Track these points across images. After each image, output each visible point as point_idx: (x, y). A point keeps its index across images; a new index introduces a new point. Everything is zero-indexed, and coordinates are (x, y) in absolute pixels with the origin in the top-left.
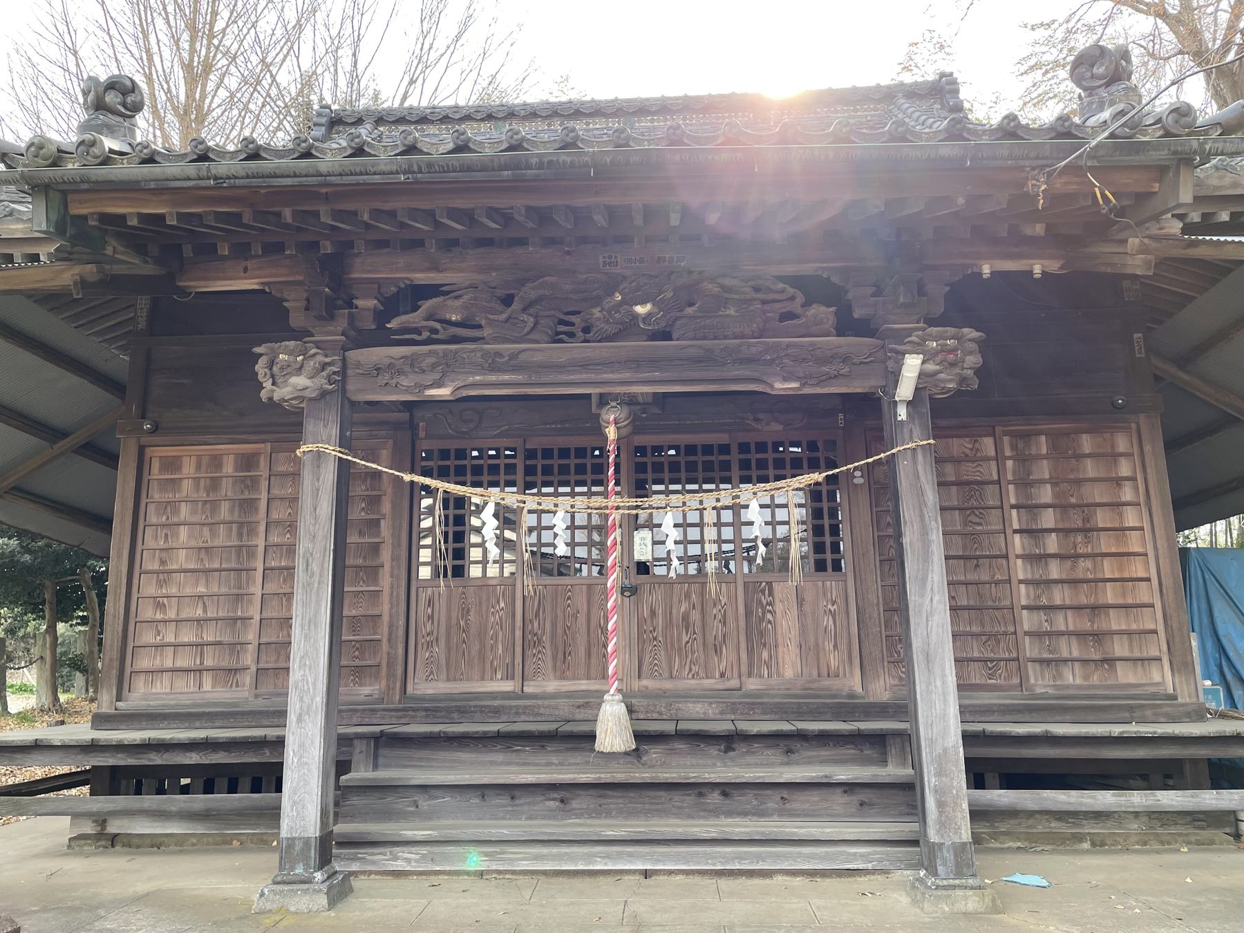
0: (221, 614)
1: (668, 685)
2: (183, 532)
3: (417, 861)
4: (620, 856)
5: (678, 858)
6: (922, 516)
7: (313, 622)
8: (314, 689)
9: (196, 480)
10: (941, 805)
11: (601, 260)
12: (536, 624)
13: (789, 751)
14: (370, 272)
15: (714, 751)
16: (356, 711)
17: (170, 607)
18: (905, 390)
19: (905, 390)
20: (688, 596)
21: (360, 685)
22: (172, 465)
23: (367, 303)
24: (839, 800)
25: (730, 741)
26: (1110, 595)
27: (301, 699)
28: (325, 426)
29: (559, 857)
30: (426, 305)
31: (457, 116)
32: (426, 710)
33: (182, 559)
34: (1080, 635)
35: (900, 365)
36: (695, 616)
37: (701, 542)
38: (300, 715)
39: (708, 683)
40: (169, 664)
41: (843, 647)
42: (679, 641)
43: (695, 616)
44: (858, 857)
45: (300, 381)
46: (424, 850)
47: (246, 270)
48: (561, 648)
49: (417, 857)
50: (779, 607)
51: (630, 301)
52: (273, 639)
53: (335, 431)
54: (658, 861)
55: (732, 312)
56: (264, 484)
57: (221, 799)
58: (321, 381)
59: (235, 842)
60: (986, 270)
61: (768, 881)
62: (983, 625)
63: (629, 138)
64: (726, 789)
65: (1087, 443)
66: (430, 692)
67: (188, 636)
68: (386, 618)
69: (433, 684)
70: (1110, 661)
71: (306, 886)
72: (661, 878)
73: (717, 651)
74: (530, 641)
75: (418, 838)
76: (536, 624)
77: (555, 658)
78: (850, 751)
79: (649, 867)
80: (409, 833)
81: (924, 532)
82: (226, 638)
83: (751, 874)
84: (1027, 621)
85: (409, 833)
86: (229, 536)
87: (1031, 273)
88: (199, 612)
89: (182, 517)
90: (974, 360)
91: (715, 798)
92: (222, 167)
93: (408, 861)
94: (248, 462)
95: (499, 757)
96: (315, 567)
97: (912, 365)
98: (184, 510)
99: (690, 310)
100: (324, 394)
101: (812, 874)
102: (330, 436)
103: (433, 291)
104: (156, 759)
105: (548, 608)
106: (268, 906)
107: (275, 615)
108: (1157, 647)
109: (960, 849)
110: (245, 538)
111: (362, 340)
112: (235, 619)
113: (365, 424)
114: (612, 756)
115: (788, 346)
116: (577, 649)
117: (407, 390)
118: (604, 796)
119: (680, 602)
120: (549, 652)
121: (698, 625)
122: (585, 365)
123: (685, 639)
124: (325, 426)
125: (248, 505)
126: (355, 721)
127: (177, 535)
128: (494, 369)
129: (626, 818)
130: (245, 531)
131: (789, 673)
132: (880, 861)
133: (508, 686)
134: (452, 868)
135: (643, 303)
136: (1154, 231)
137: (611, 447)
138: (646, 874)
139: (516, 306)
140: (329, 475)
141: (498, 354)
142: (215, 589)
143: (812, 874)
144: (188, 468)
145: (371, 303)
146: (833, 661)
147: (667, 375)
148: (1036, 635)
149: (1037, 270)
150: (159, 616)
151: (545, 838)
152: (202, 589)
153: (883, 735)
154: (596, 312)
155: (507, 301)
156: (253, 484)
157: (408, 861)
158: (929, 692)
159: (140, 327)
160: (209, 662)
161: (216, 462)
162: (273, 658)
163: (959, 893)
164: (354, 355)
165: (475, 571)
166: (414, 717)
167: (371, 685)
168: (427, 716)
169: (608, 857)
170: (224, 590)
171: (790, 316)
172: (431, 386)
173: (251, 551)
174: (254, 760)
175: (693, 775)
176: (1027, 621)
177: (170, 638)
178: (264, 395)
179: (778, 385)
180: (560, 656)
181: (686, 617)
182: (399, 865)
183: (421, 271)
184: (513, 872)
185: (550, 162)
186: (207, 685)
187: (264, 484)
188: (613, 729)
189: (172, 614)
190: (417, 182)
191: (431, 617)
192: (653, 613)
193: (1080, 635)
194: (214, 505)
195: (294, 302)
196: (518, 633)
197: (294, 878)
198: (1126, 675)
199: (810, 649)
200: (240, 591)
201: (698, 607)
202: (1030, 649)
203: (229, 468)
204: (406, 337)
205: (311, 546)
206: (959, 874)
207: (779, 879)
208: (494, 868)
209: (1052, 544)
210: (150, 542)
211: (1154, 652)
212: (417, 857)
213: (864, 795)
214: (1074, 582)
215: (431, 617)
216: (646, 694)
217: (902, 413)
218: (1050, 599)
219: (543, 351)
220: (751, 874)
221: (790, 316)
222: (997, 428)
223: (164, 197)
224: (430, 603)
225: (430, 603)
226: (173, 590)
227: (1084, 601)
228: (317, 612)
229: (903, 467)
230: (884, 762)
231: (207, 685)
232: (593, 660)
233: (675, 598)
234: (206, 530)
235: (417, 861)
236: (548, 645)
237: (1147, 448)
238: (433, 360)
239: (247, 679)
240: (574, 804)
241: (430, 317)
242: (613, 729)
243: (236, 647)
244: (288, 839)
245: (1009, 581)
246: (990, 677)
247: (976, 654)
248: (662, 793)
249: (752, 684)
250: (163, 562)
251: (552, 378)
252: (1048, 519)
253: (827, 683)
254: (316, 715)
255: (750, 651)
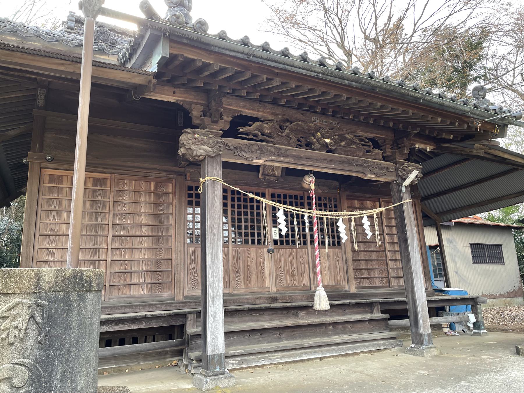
0: (87, 258)
3: (236, 364)
5: (332, 351)
6: (411, 225)
8: (218, 286)
11: (313, 119)
12: (236, 264)
14: (229, 105)
16: (162, 304)
17: (57, 253)
19: (407, 183)
20: (291, 254)
21: (162, 292)
27: (213, 291)
28: (216, 170)
29: (290, 356)
32: (195, 302)
36: (294, 262)
38: (213, 298)
41: (342, 273)
42: (289, 272)
46: (239, 359)
47: (174, 92)
48: (246, 274)
49: (236, 362)
51: (323, 137)
52: (117, 271)
54: (323, 353)
57: (128, 348)
59: (105, 373)
60: (417, 146)
61: (358, 356)
62: (378, 266)
63: (389, 80)
66: (194, 294)
69: (195, 291)
71: (223, 376)
72: (326, 359)
73: (302, 275)
75: (236, 354)
76: (236, 264)
77: (244, 278)
79: (321, 356)
80: (232, 352)
81: (412, 231)
83: (353, 354)
85: (232, 352)
86: (91, 219)
87: (426, 150)
89: (64, 207)
92: (270, 55)
93: (233, 364)
95: (247, 319)
96: (215, 231)
101: (370, 352)
102: (218, 174)
103: (256, 120)
105: (241, 258)
106: (211, 387)
107: (118, 259)
109: (429, 335)
110: (100, 220)
112: (95, 261)
113: (165, 171)
115: (371, 162)
117: (246, 159)
118: (294, 331)
119: (289, 256)
121: (295, 265)
122: (311, 159)
123: (291, 271)
124: (216, 170)
126: (163, 308)
127: (61, 216)
128: (278, 155)
129: (302, 339)
130: (99, 217)
132: (388, 345)
134: (251, 365)
135: (328, 138)
136: (486, 143)
137: (248, 194)
138: (321, 359)
143: (370, 352)
147: (336, 167)
149: (428, 149)
150: (50, 258)
151: (285, 349)
157: (233, 364)
158: (418, 284)
159: (40, 105)
162: (118, 280)
163: (432, 349)
166: (190, 306)
167: (167, 292)
168: (196, 305)
169: (307, 353)
170: (88, 246)
172: (256, 158)
174: (137, 327)
179: (369, 176)
180: (246, 278)
181: (291, 262)
183: (249, 109)
184: (275, 364)
185: (369, 82)
188: (321, 301)
190: (317, 78)
191: (193, 261)
195: (196, 113)
197: (217, 373)
200: (97, 247)
201: (295, 258)
204: (244, 136)
205: (213, 222)
206: (429, 344)
207: (362, 355)
208: (267, 363)
212: (236, 362)
213: (373, 323)
215: (193, 261)
218: (396, 257)
220: (353, 354)
222: (381, 199)
223: (212, 56)
228: (217, 252)
229: (405, 207)
230: (372, 312)
232: (259, 279)
233: (287, 255)
235: (236, 364)
236: (241, 274)
238: (257, 147)
241: (258, 129)
242: (321, 301)
244: (211, 355)
245: (385, 251)
246: (381, 283)
247: (377, 276)
248: (313, 328)
250: (52, 230)
251: (303, 162)
254: (220, 298)
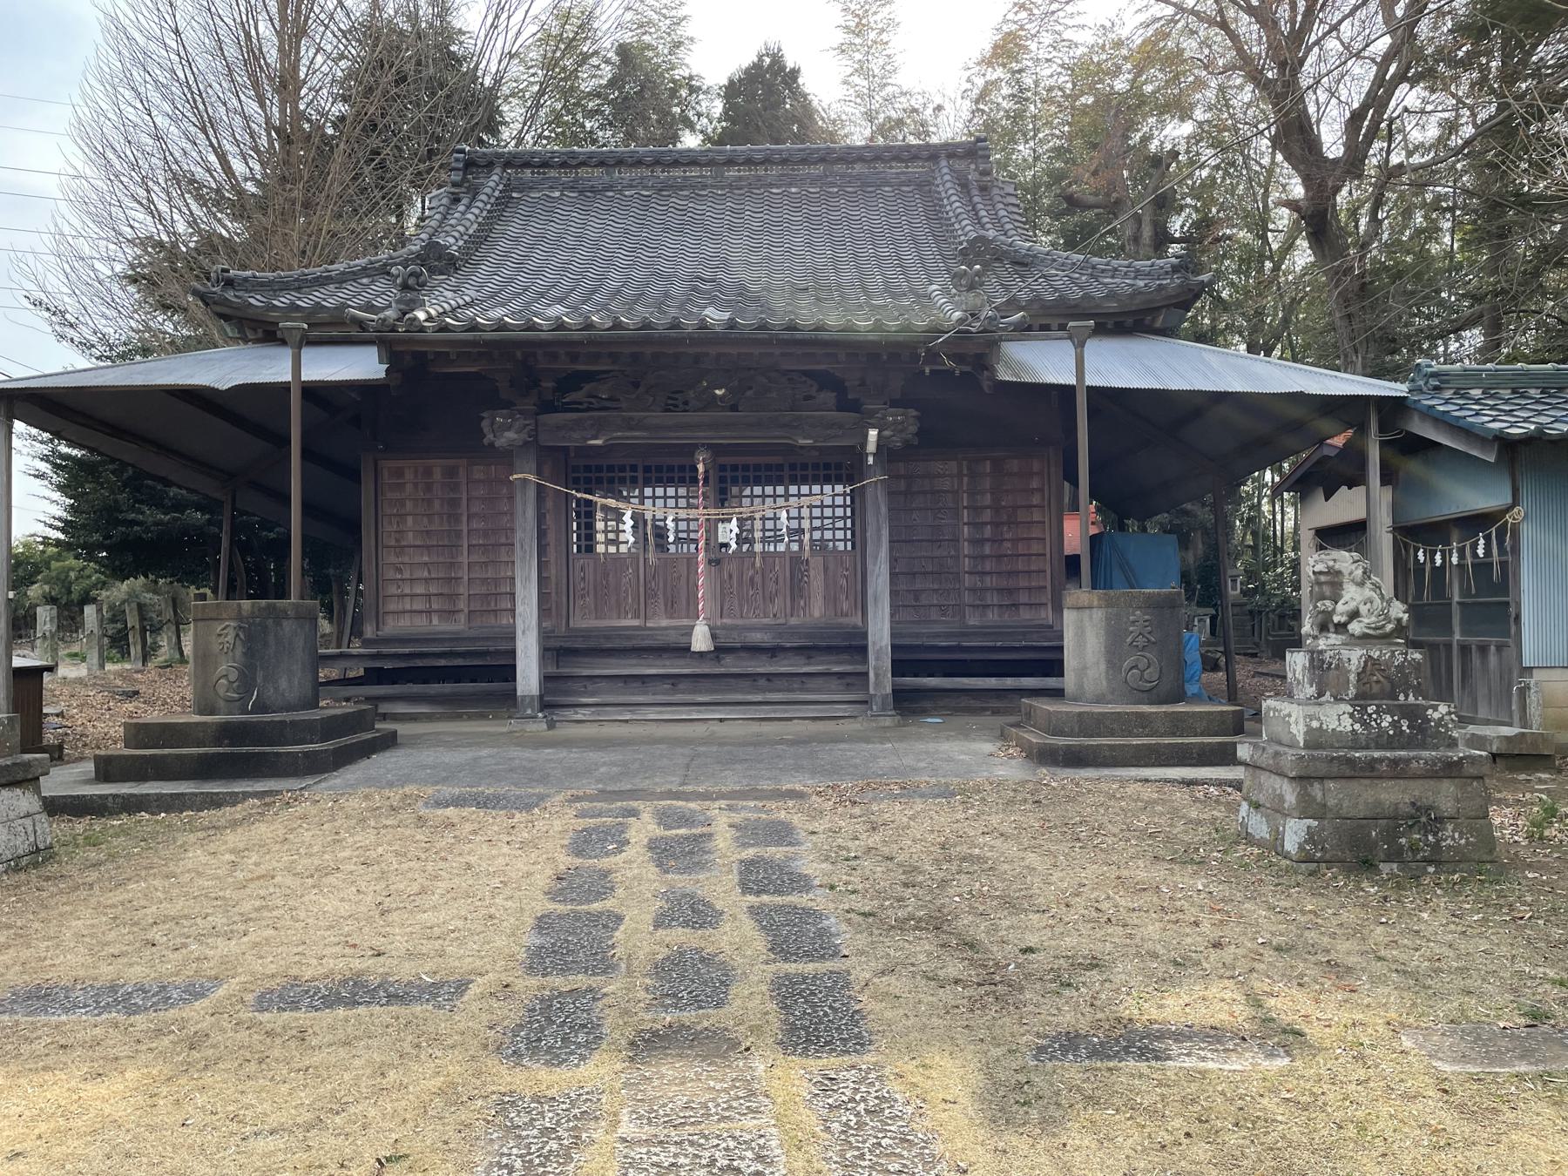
1: (740, 622)
2: (410, 520)
4: (706, 712)
7: (528, 579)
9: (416, 485)
10: (877, 675)
13: (809, 658)
15: (764, 657)
18: (871, 447)
19: (871, 447)
22: (399, 473)
23: (548, 384)
24: (834, 683)
25: (773, 651)
26: (1020, 565)
30: (587, 387)
31: (574, 162)
33: (410, 538)
34: (1000, 590)
35: (867, 436)
36: (758, 579)
37: (812, 518)
39: (766, 621)
40: (408, 607)
41: (852, 598)
43: (758, 579)
44: (840, 710)
45: (511, 435)
50: (812, 573)
53: (534, 466)
55: (774, 395)
56: (464, 488)
58: (524, 436)
64: (769, 677)
65: (1014, 465)
67: (420, 590)
68: (553, 579)
70: (1016, 606)
73: (772, 601)
74: (650, 594)
78: (846, 657)
81: (879, 530)
82: (446, 591)
84: (968, 581)
88: (426, 574)
90: (913, 429)
91: (762, 682)
94: (451, 472)
95: (634, 662)
97: (873, 433)
98: (409, 505)
99: (749, 393)
100: (526, 443)
104: (419, 663)
108: (1047, 597)
111: (548, 407)
114: (701, 654)
116: (682, 602)
120: (661, 601)
125: (454, 503)
131: (817, 614)
133: (636, 623)
138: (721, 720)
139: (641, 389)
140: (531, 493)
141: (631, 418)
142: (435, 559)
144: (409, 476)
145: (550, 385)
146: (845, 606)
148: (973, 590)
152: (426, 559)
153: (856, 647)
154: (691, 394)
155: (636, 385)
156: (455, 487)
160: (435, 606)
161: (428, 472)
164: (545, 418)
165: (600, 549)
171: (808, 398)
173: (458, 534)
175: (750, 670)
176: (968, 581)
177: (407, 591)
178: (486, 441)
181: (752, 579)
182: (579, 717)
186: (435, 621)
187: (464, 488)
189: (407, 575)
191: (583, 579)
192: (730, 576)
193: (1000, 590)
194: (430, 502)
196: (642, 590)
198: (1026, 615)
199: (831, 599)
202: (967, 598)
203: (437, 475)
209: (988, 532)
210: (388, 528)
211: (1044, 600)
214: (999, 557)
215: (583, 579)
216: (724, 627)
217: (871, 460)
219: (657, 417)
221: (808, 398)
224: (582, 569)
225: (582, 569)
226: (406, 560)
227: (1004, 568)
229: (869, 492)
231: (435, 621)
234: (425, 520)
237: (1053, 469)
239: (462, 617)
240: (681, 686)
242: (701, 640)
243: (452, 597)
249: (793, 621)
252: (987, 516)
253: (841, 620)
255: (793, 600)
